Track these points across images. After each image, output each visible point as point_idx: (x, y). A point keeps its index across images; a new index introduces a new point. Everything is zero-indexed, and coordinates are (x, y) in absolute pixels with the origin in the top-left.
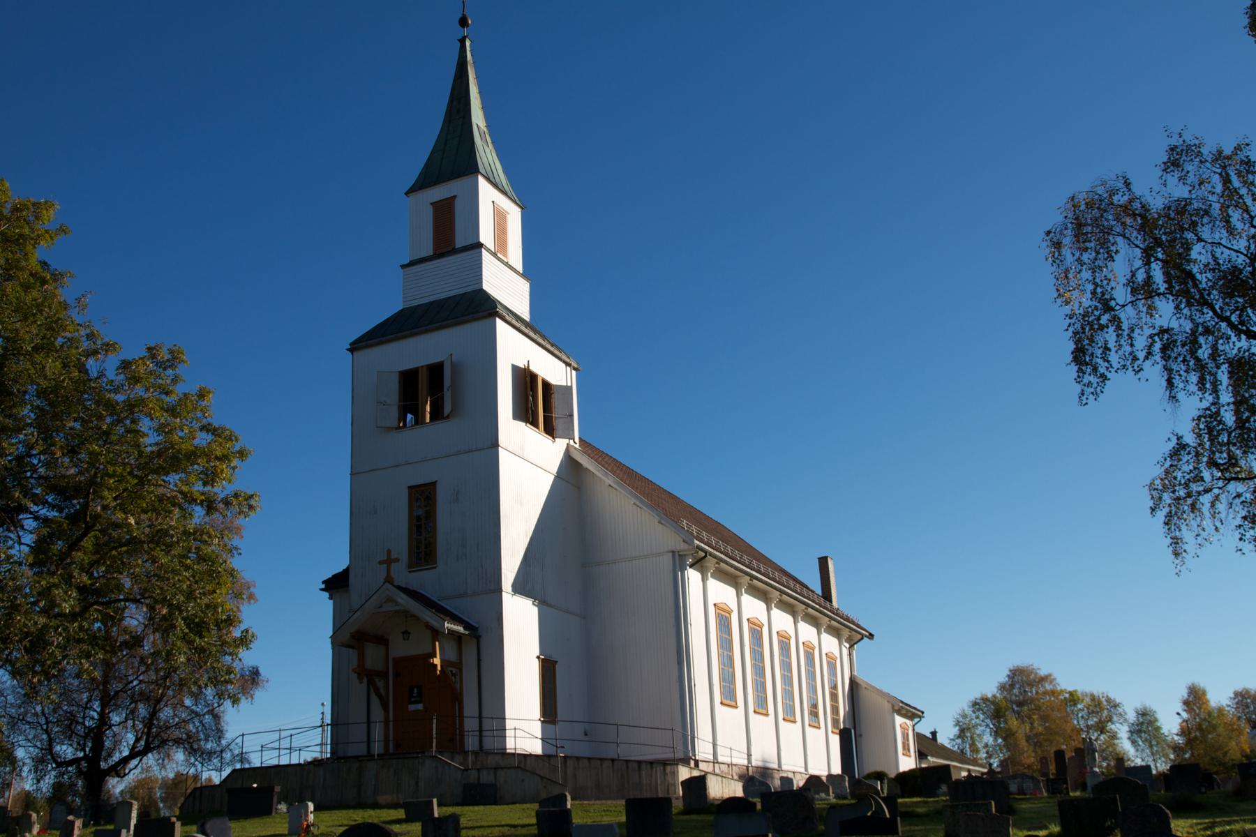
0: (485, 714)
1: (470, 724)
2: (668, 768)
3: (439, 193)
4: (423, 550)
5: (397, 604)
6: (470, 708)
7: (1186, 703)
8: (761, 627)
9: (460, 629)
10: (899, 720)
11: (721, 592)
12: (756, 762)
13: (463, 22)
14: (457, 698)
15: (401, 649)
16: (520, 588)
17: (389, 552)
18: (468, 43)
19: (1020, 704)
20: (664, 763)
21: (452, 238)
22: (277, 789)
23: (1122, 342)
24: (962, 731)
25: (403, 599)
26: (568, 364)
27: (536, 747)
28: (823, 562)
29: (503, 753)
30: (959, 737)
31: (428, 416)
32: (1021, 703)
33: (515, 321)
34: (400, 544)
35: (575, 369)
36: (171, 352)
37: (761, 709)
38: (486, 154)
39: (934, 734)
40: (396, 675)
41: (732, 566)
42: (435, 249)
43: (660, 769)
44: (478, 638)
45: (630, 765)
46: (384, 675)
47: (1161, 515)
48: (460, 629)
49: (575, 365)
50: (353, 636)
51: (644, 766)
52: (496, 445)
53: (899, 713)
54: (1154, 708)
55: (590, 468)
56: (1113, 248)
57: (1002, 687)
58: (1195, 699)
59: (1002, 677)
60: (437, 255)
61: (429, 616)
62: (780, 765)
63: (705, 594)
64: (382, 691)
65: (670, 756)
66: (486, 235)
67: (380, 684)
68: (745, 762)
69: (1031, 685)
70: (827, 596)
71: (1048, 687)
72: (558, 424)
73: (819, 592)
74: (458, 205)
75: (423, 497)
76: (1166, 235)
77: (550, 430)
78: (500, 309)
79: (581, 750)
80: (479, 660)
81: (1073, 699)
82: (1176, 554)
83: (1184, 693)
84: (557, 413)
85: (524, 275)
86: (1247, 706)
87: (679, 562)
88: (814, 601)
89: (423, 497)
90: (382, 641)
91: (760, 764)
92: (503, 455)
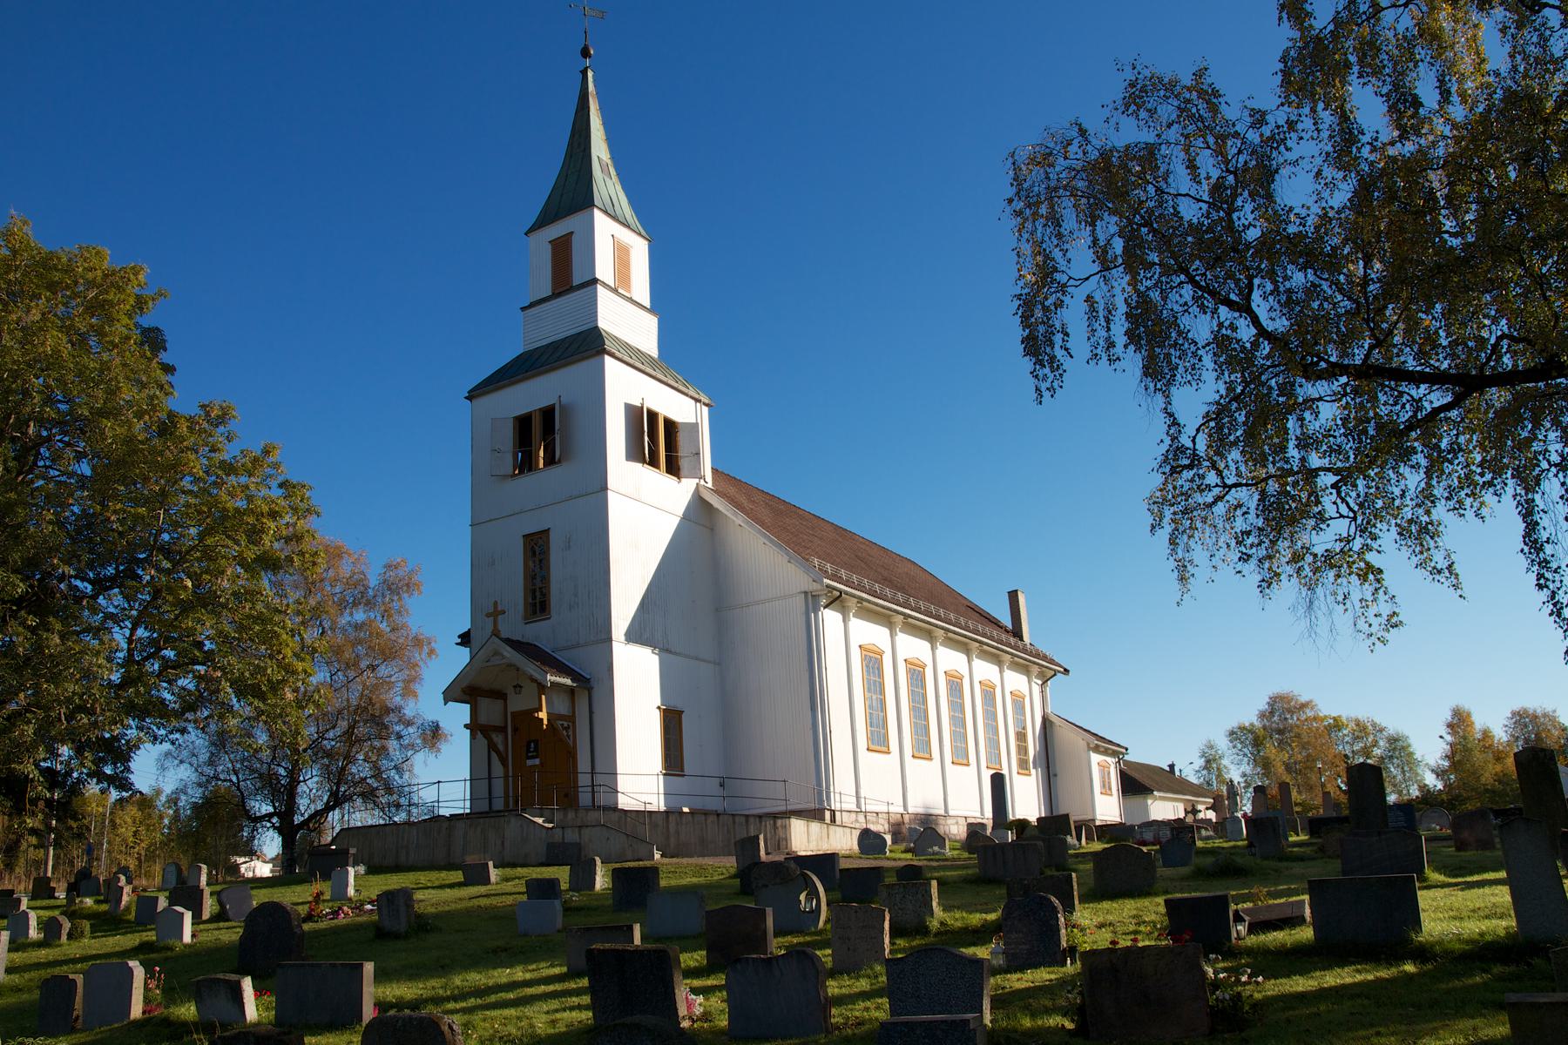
1: (584, 780)
2: (779, 822)
3: (556, 230)
4: (538, 603)
5: (504, 657)
6: (583, 764)
7: (1450, 726)
9: (568, 681)
10: (1096, 758)
11: (867, 632)
12: (916, 806)
13: (585, 53)
14: (571, 754)
15: (517, 704)
16: (636, 635)
18: (590, 74)
19: (1280, 732)
20: (775, 816)
21: (569, 276)
22: (353, 851)
23: (1096, 326)
24: (1208, 762)
25: (509, 653)
26: (697, 401)
27: (657, 803)
28: (1013, 596)
29: (615, 809)
30: (1205, 768)
32: (1280, 730)
33: (634, 359)
34: (514, 593)
36: (222, 408)
37: (923, 750)
38: (607, 184)
39: (1172, 766)
40: (515, 730)
42: (554, 289)
43: (769, 823)
44: (590, 690)
46: (502, 729)
47: (1164, 533)
48: (568, 681)
50: (464, 691)
51: (751, 820)
52: (605, 488)
53: (1097, 749)
54: (1406, 733)
55: (721, 508)
57: (1262, 715)
58: (1459, 722)
59: (1262, 704)
60: (556, 295)
61: (531, 668)
62: (946, 810)
63: (845, 637)
64: (501, 747)
65: (783, 808)
66: (604, 268)
67: (498, 739)
69: (1291, 712)
70: (1017, 633)
71: (1310, 713)
72: (684, 464)
73: (1010, 626)
75: (537, 546)
76: (1114, 182)
77: (673, 469)
78: (609, 345)
79: (714, 804)
80: (591, 713)
81: (1337, 724)
82: (1182, 579)
83: (1448, 716)
84: (683, 449)
85: (652, 310)
86: (1526, 726)
87: (812, 602)
88: (1000, 635)
89: (537, 546)
90: (500, 695)
91: (921, 811)
92: (612, 498)
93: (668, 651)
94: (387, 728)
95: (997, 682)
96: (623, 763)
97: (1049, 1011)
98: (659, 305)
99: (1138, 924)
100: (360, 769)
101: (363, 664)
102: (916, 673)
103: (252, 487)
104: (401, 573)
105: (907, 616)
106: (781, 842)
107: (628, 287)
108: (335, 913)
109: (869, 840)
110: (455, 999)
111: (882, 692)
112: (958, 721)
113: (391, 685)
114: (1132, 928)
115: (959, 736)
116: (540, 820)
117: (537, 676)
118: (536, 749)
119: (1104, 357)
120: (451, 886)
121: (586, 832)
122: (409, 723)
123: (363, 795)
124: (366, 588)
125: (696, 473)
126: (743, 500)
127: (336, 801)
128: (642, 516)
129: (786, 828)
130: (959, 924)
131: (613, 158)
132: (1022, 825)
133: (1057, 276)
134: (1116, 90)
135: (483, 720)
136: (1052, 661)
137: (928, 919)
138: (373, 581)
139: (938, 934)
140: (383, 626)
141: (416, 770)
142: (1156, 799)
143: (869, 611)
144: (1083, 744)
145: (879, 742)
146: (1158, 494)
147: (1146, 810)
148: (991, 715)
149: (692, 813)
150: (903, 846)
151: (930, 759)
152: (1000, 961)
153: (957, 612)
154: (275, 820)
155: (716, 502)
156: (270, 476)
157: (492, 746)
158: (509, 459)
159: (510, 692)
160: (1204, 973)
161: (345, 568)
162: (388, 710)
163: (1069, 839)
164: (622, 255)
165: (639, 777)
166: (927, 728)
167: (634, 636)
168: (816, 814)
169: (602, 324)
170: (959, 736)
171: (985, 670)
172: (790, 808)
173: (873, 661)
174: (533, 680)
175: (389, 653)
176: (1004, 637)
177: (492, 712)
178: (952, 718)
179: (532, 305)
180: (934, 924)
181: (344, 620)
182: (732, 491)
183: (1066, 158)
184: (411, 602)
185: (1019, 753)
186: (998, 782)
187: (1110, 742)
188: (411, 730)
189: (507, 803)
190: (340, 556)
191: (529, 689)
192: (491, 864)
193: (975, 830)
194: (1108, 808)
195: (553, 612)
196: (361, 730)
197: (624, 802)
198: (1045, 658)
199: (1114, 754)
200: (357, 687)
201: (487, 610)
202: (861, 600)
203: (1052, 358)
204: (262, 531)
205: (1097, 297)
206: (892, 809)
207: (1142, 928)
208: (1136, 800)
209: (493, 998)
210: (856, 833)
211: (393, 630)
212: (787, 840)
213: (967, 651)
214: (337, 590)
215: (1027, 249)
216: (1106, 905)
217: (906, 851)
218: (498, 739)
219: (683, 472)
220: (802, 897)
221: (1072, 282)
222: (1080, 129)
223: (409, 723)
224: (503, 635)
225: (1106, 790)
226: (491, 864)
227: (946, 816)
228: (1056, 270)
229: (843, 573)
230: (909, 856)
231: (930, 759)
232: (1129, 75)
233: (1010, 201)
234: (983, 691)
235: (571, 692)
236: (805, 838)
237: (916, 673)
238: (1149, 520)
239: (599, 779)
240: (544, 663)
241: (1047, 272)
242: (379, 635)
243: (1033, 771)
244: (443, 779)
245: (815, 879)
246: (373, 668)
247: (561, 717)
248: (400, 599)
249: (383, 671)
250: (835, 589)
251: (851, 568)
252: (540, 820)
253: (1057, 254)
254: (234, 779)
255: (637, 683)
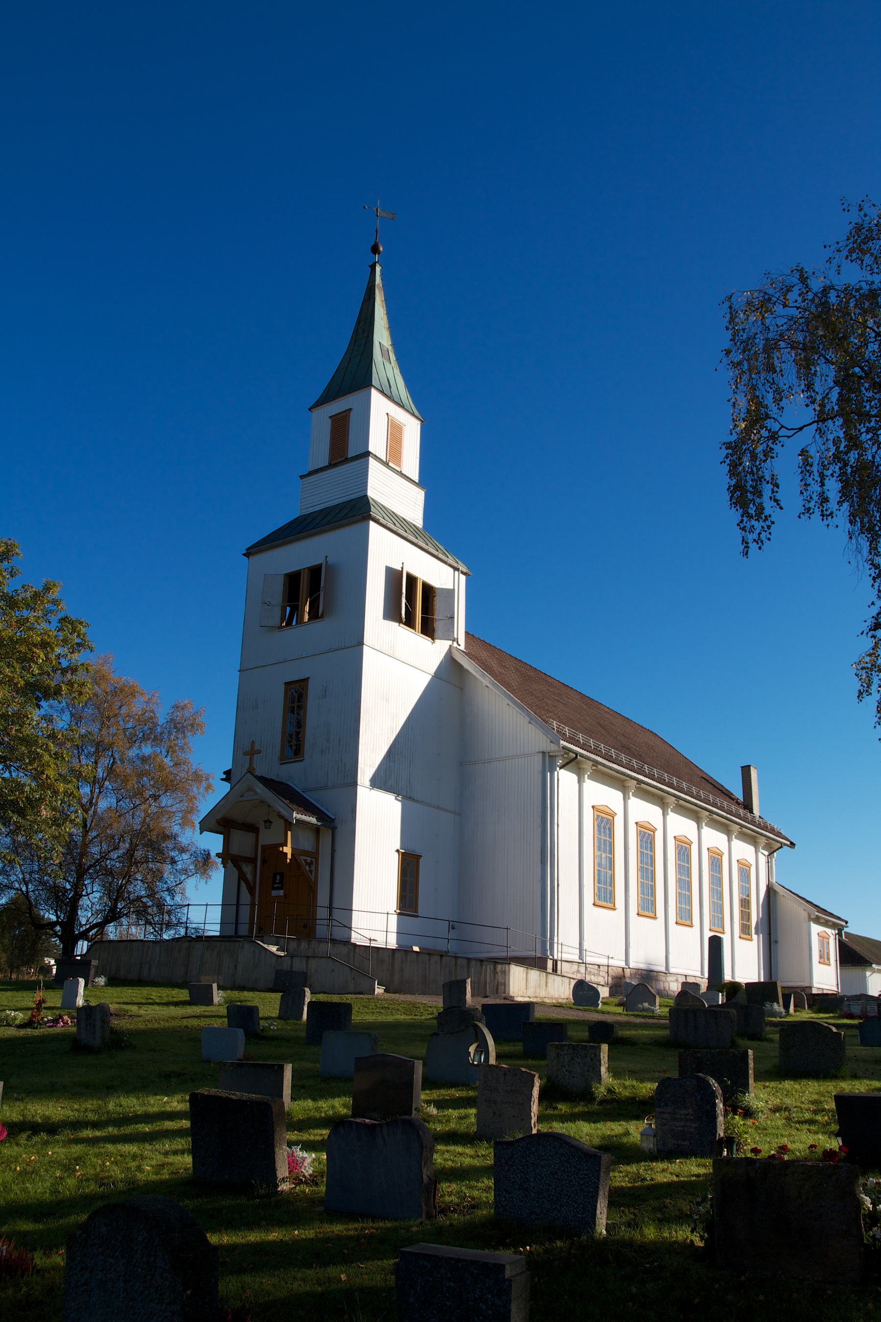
0: (335, 905)
1: (322, 913)
2: (499, 967)
4: (294, 744)
5: (256, 793)
6: (322, 898)
8: (654, 830)
9: (313, 820)
10: (816, 929)
12: (637, 961)
13: (375, 250)
14: (312, 889)
15: (267, 838)
17: (253, 743)
18: (378, 269)
20: (495, 961)
21: (346, 449)
23: (810, 480)
25: (260, 789)
26: (456, 569)
28: (746, 771)
29: (347, 942)
31: (306, 617)
33: (398, 526)
35: (462, 573)
37: (647, 909)
38: (385, 367)
40: (264, 861)
41: (611, 769)
42: (331, 460)
43: (489, 967)
44: (334, 830)
45: (459, 961)
46: (252, 861)
48: (313, 820)
49: (465, 570)
50: (218, 823)
51: (473, 963)
52: (361, 643)
53: (817, 921)
56: (738, 357)
60: (332, 465)
61: (279, 805)
63: (578, 799)
64: (249, 877)
65: (504, 954)
66: (377, 443)
67: (247, 869)
68: (623, 964)
70: (748, 805)
72: (439, 626)
73: (741, 799)
74: (353, 416)
75: (296, 695)
77: (428, 630)
78: (374, 512)
79: (441, 945)
84: (439, 613)
85: (420, 484)
87: (549, 763)
88: (728, 805)
89: (296, 695)
90: (252, 828)
91: (642, 966)
93: (410, 798)
94: (161, 852)
95: (694, 838)
96: (359, 900)
97: (682, 1218)
98: (427, 479)
99: (815, 1112)
100: (138, 889)
101: (147, 794)
102: (646, 836)
103: (32, 620)
104: (186, 713)
105: (640, 782)
106: (501, 986)
107: (398, 461)
108: (55, 1021)
109: (584, 992)
110: (95, 1125)
111: (612, 851)
112: (684, 884)
113: (171, 815)
114: (807, 1116)
115: (684, 898)
116: (273, 949)
117: (284, 813)
118: (281, 882)
119: (817, 513)
120: (176, 1004)
121: (313, 963)
122: (183, 850)
123: (138, 913)
124: (156, 725)
125: (449, 635)
126: (494, 664)
127: (112, 916)
128: (395, 674)
129: (506, 974)
130: (626, 1093)
131: (394, 345)
132: (734, 988)
133: (769, 423)
134: (840, 229)
135: (234, 850)
136: (779, 834)
137: (594, 1085)
138: (162, 719)
139: (603, 1102)
140: (168, 761)
141: (188, 893)
142: (874, 971)
143: (604, 774)
144: (804, 915)
145: (605, 897)
146: (867, 659)
147: (864, 982)
148: (716, 881)
149: (424, 952)
150: (616, 1000)
151: (655, 918)
152: (649, 1145)
153: (691, 782)
154: (58, 928)
155: (467, 664)
156: (51, 611)
157: (242, 877)
158: (277, 612)
159: (262, 826)
160: (859, 1203)
161: (137, 706)
162: (167, 837)
163: (775, 1006)
164: (395, 432)
165: (374, 913)
166: (653, 889)
167: (380, 782)
168: (539, 961)
169: (371, 493)
170: (684, 898)
171: (713, 838)
172: (510, 954)
173: (604, 821)
174: (281, 817)
175: (170, 785)
176: (734, 808)
177: (243, 843)
178: (679, 881)
179: (311, 473)
180: (601, 1091)
181: (132, 753)
182: (484, 655)
183: (785, 306)
184: (194, 741)
185: (742, 918)
186: (715, 945)
187: (831, 915)
188: (185, 856)
189: (251, 930)
190: (133, 694)
191: (278, 824)
192: (215, 986)
193: (688, 988)
194: (825, 978)
195: (307, 756)
196: (139, 854)
197: (357, 938)
198: (772, 830)
199: (833, 926)
200: (140, 814)
201: (246, 750)
202: (596, 763)
203: (760, 509)
204: (32, 660)
205: (812, 451)
206: (611, 962)
207: (819, 1118)
208: (853, 972)
209: (128, 1130)
210: (573, 982)
211: (176, 764)
212: (505, 985)
213: (698, 819)
214: (130, 725)
215: (743, 403)
216: (787, 1084)
217: (619, 1005)
218: (247, 869)
219: (436, 634)
220: (472, 1049)
221: (783, 432)
222: (801, 276)
223: (183, 850)
224: (258, 773)
225: (824, 959)
226: (215, 986)
227: (667, 973)
228: (768, 417)
229: (581, 737)
230: (620, 1010)
231: (655, 918)
232: (854, 217)
233: (728, 352)
234: (710, 857)
235: (317, 830)
236: (522, 985)
237: (646, 836)
238: (857, 685)
239: (336, 914)
240: (292, 801)
241: (757, 417)
242: (161, 767)
243: (755, 937)
244: (202, 903)
245: (486, 1032)
246: (156, 797)
247: (306, 853)
248: (185, 737)
249: (165, 801)
250: (571, 750)
251: (589, 733)
252: (273, 949)
253: (769, 399)
254: (24, 889)
255: (378, 826)
